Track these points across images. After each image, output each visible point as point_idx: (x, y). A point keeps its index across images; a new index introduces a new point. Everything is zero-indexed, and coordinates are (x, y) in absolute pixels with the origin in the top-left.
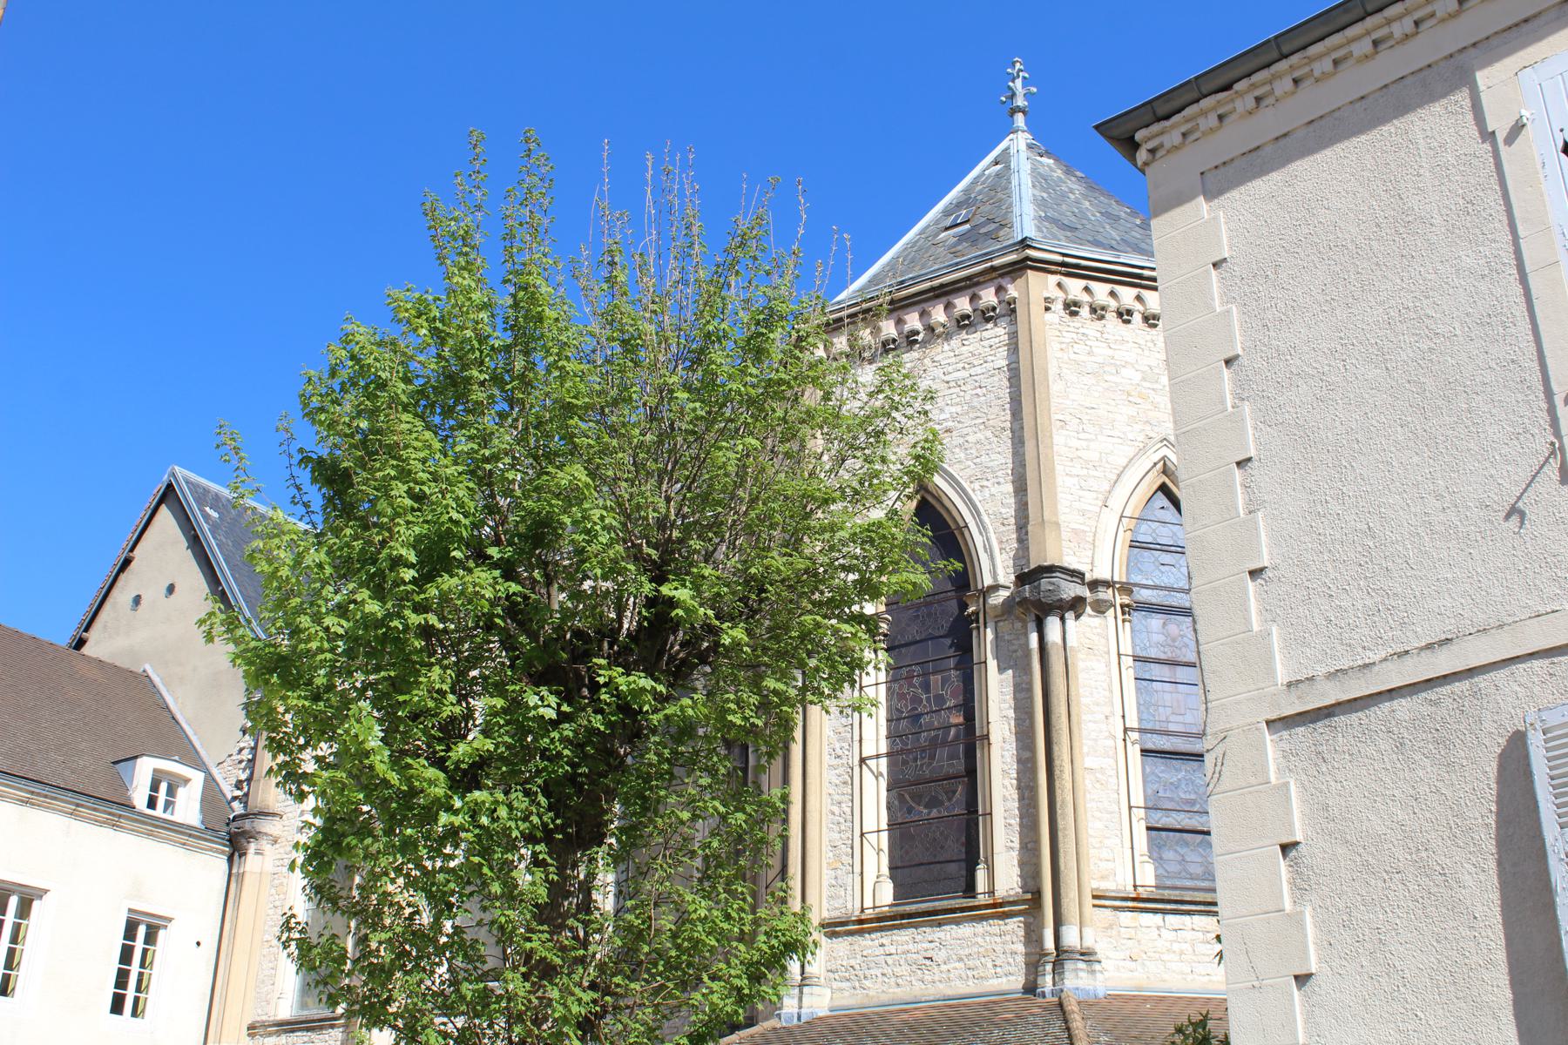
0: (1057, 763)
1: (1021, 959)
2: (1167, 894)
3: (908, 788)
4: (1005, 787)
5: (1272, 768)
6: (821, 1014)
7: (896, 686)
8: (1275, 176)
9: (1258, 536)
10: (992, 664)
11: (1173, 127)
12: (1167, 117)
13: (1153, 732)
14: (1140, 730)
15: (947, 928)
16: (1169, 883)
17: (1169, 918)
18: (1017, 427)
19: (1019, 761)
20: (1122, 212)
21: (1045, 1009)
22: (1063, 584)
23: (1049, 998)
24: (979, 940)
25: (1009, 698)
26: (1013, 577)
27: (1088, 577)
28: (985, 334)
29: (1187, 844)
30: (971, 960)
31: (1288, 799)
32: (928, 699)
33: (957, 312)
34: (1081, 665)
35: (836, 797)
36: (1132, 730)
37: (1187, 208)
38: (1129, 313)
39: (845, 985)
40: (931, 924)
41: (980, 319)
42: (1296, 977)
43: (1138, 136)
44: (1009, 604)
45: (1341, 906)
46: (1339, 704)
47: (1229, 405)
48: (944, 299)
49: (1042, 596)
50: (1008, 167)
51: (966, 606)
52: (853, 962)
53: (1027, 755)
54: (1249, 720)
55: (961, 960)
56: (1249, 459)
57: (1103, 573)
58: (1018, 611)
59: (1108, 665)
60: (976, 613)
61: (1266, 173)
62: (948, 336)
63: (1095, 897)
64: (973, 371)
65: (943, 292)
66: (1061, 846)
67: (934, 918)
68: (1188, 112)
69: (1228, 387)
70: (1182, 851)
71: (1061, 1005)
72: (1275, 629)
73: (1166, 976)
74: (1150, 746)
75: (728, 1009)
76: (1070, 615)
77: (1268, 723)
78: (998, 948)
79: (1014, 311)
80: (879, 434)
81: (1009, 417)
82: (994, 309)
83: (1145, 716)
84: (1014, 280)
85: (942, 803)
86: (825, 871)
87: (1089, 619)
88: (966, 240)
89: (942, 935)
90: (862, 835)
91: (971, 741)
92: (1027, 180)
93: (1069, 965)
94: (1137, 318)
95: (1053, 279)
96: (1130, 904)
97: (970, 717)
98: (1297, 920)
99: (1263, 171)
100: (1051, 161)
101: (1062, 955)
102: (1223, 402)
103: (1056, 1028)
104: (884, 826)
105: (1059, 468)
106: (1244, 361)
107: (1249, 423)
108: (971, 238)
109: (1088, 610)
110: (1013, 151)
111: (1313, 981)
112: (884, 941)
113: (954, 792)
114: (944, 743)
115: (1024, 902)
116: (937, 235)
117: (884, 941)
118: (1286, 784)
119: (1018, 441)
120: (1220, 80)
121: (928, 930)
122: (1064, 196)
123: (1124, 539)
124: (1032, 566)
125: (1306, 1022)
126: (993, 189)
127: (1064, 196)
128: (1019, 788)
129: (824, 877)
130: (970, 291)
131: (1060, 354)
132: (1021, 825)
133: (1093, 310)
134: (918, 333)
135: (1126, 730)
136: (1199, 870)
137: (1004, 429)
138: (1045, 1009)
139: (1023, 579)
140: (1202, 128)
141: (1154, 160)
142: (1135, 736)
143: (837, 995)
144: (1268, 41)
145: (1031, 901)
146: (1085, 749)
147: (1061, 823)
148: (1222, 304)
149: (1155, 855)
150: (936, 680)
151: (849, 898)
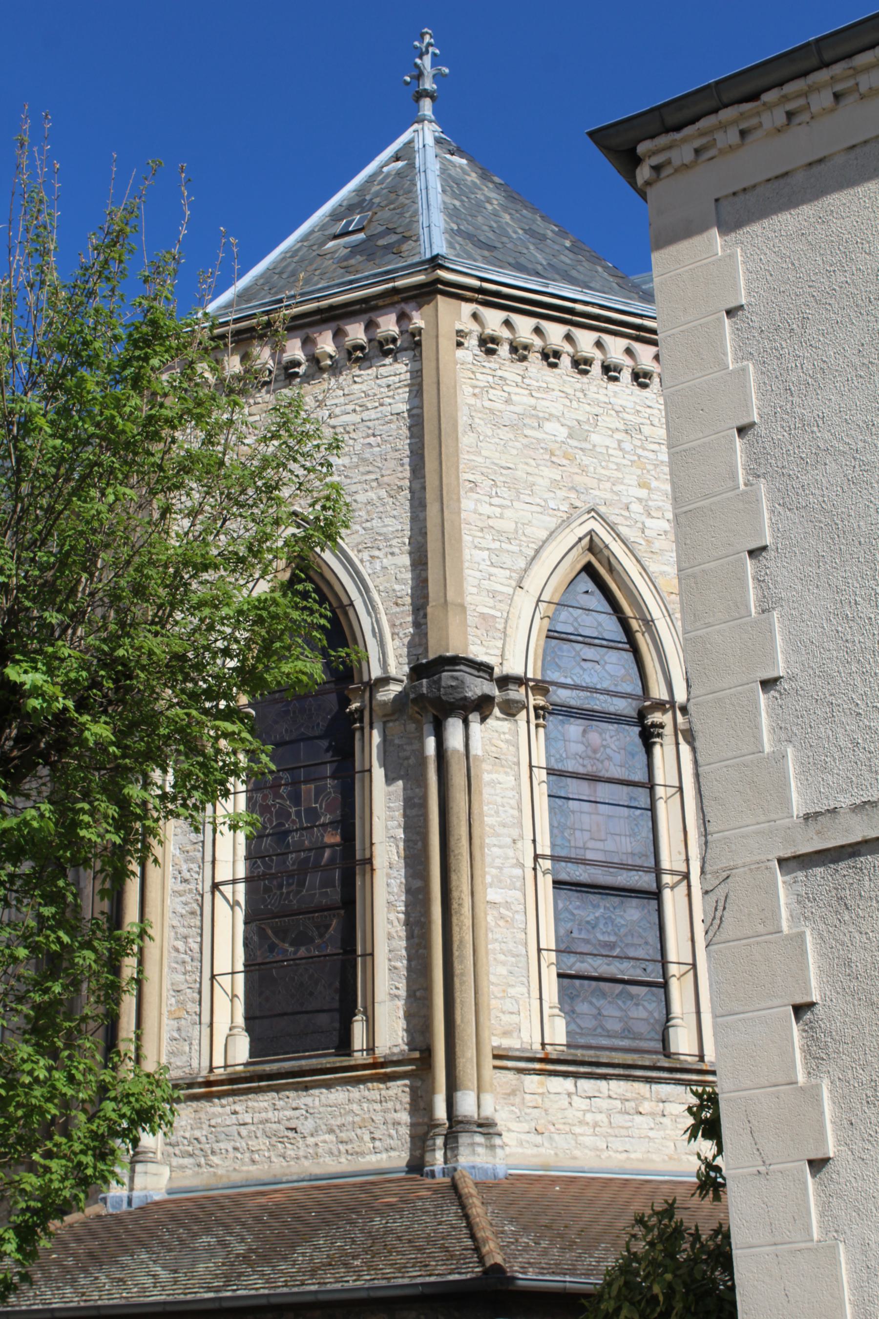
0: (455, 894)
1: (405, 1131)
2: (579, 1054)
3: (267, 922)
4: (390, 922)
5: (784, 913)
6: (157, 1198)
7: (259, 796)
8: (807, 210)
9: (773, 639)
10: (378, 773)
11: (684, 140)
12: (678, 128)
13: (568, 860)
14: (554, 858)
15: (316, 1092)
16: (582, 1041)
17: (583, 1083)
18: (416, 486)
19: (409, 891)
20: (550, 230)
21: (435, 1192)
22: (468, 679)
23: (440, 1179)
24: (355, 1107)
25: (398, 814)
26: (406, 669)
27: (497, 672)
28: (383, 371)
29: (604, 995)
30: (348, 1132)
31: (804, 952)
32: (298, 814)
33: (349, 341)
34: (486, 777)
35: (182, 931)
36: (544, 857)
37: (697, 241)
38: (557, 354)
39: (187, 1161)
40: (296, 1087)
41: (377, 352)
42: (811, 1162)
43: (641, 149)
44: (400, 698)
45: (865, 1078)
46: (866, 842)
47: (741, 481)
48: (334, 325)
49: (442, 692)
50: (411, 165)
51: (348, 702)
52: (197, 1133)
53: (418, 883)
54: (757, 858)
55: (331, 1131)
56: (764, 548)
57: (514, 667)
58: (412, 709)
59: (518, 778)
60: (360, 711)
61: (796, 205)
62: (335, 369)
63: (496, 1057)
64: (366, 415)
65: (333, 316)
66: (457, 994)
67: (300, 1080)
68: (703, 123)
69: (740, 459)
70: (600, 1003)
71: (454, 1186)
72: (790, 751)
73: (577, 1153)
74: (563, 877)
75: (67, 1193)
76: (474, 717)
77: (781, 861)
78: (378, 1118)
79: (418, 344)
80: (271, 488)
81: (407, 474)
82: (394, 340)
83: (559, 841)
84: (420, 307)
85: (312, 940)
86: (165, 1020)
87: (497, 723)
88: (361, 253)
89: (308, 1100)
90: (213, 977)
91: (351, 864)
92: (435, 184)
93: (464, 1139)
94: (565, 361)
95: (467, 308)
96: (537, 1066)
97: (349, 837)
98: (812, 1095)
99: (791, 202)
100: (464, 161)
101: (456, 1126)
102: (734, 477)
103: (451, 1214)
104: (240, 967)
105: (467, 539)
106: (761, 430)
107: (765, 504)
108: (368, 250)
109: (496, 711)
110: (418, 145)
111: (830, 1167)
112: (237, 1108)
113: (328, 927)
114: (317, 866)
115: (410, 1061)
116: (324, 243)
117: (237, 1108)
118: (802, 935)
119: (418, 504)
120: (745, 88)
121: (292, 1094)
122: (479, 206)
123: (540, 627)
124: (432, 656)
125: (822, 1215)
126: (393, 190)
127: (479, 206)
128: (407, 923)
129: (165, 1029)
130: (366, 317)
131: (472, 401)
132: (409, 969)
133: (514, 349)
134: (298, 364)
135: (536, 857)
136: (617, 1027)
137: (401, 488)
138: (435, 1192)
139: (418, 671)
140: (720, 145)
141: (658, 179)
142: (547, 864)
143: (178, 1174)
144: (808, 44)
145: (417, 1065)
146: (488, 879)
147: (458, 968)
148: (736, 360)
149: (567, 1008)
150: (307, 789)
151: (195, 1055)
